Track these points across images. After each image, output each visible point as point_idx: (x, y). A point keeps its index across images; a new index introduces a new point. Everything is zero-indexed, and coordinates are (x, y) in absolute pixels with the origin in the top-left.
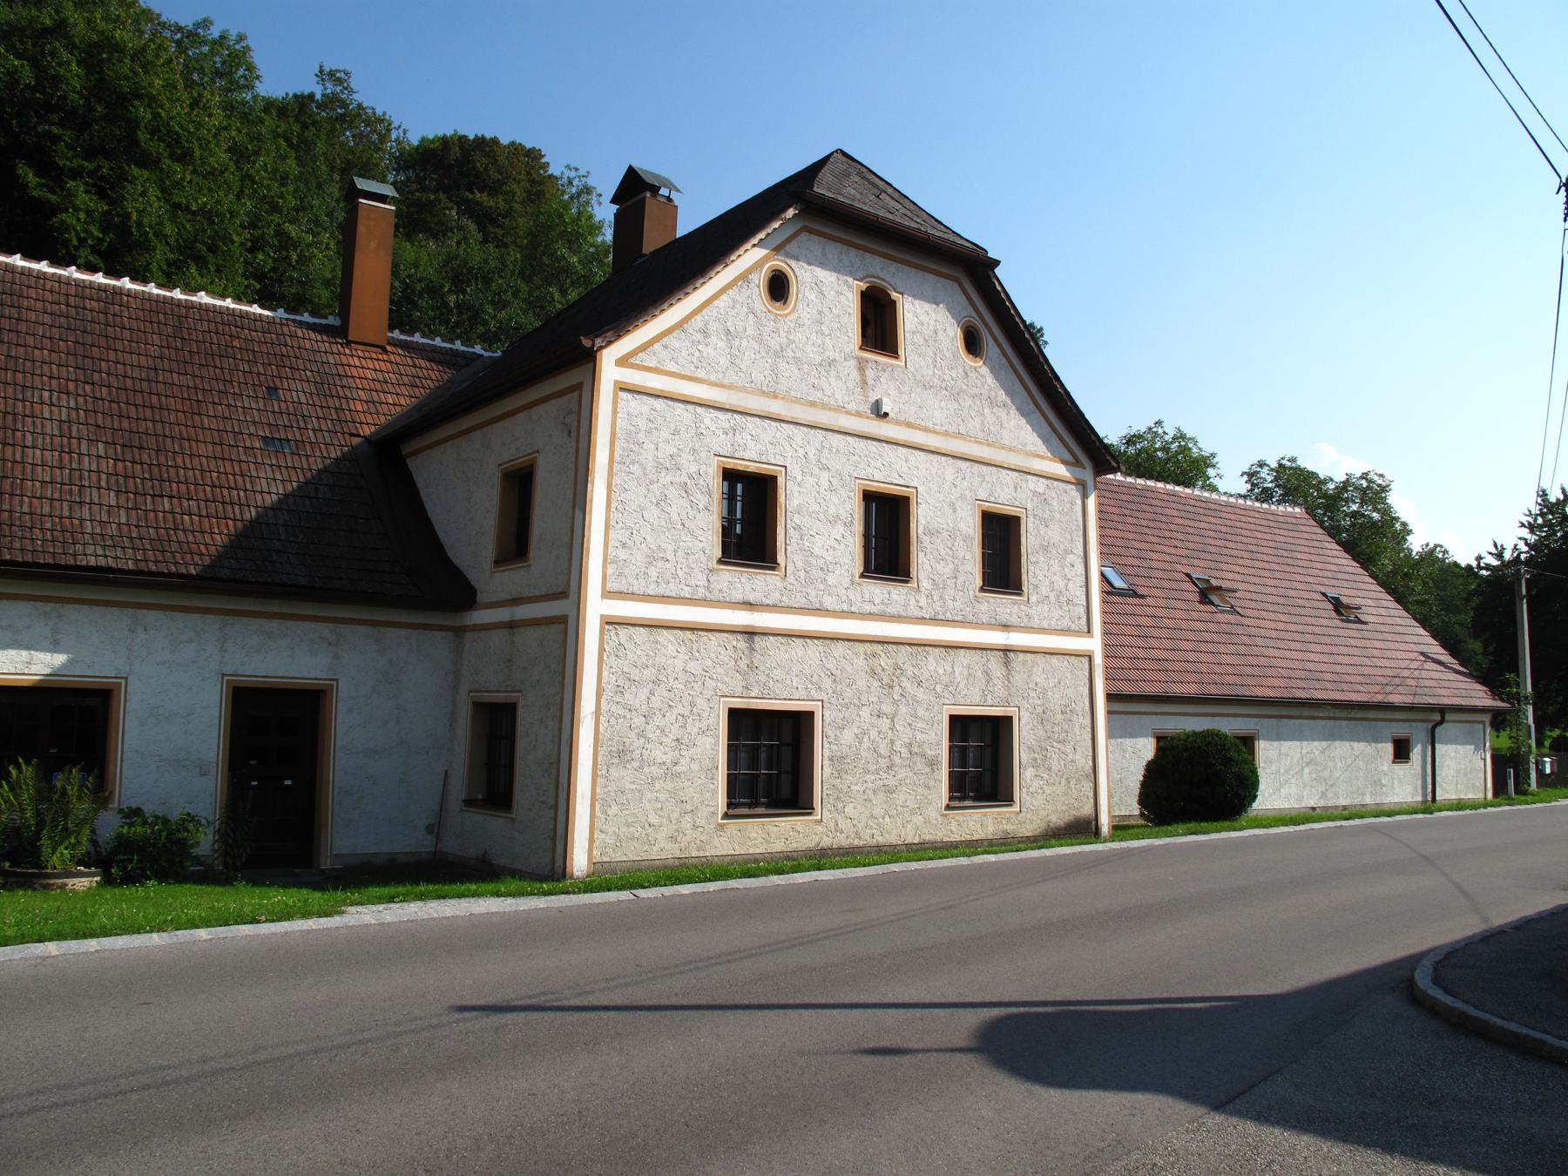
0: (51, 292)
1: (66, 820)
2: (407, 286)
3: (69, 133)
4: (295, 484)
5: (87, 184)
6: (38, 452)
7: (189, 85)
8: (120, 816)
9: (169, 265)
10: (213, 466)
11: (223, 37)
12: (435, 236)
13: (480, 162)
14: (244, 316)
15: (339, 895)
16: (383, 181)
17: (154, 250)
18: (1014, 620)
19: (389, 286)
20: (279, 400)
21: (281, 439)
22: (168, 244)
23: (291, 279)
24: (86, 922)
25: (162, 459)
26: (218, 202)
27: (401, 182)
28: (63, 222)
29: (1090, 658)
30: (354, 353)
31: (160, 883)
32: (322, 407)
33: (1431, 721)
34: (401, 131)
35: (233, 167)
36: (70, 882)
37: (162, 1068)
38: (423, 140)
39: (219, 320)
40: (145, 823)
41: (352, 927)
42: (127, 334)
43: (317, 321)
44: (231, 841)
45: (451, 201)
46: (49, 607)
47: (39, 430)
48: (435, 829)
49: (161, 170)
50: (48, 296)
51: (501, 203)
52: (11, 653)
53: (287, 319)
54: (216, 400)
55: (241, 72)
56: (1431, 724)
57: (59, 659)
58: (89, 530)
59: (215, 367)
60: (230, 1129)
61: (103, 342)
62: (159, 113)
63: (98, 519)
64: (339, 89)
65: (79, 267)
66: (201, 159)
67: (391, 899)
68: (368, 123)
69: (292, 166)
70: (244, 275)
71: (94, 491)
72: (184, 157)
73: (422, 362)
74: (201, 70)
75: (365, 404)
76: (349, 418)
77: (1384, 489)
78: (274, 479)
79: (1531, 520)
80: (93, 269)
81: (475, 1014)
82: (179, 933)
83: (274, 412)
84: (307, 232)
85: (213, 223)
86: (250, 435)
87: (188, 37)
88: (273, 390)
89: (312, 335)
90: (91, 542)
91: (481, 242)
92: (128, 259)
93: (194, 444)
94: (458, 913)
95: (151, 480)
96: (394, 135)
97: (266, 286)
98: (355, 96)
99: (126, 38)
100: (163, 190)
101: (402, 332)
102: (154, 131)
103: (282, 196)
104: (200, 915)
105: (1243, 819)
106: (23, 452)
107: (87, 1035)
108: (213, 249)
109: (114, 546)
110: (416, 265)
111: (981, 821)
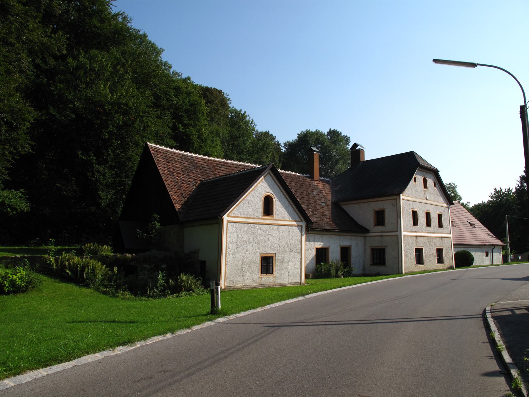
18: (442, 232)
29: (451, 238)
33: (491, 248)
46: (321, 235)
56: (492, 249)
77: (455, 187)
79: (492, 195)
105: (471, 266)
111: (440, 266)
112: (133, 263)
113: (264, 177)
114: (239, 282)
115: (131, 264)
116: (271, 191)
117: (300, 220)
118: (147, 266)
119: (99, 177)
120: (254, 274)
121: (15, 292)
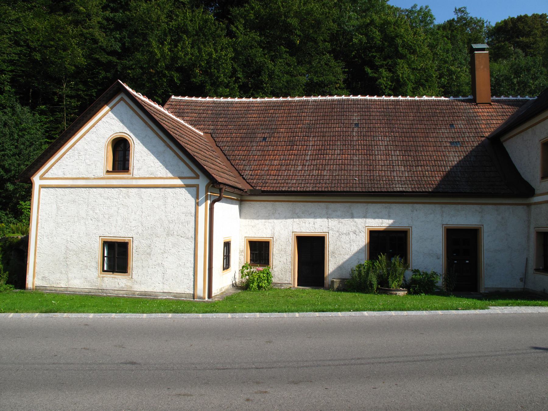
0: (378, 105)
1: (396, 273)
2: (497, 79)
3: (378, 54)
4: (462, 157)
5: (385, 68)
6: (379, 156)
7: (412, 28)
8: (412, 272)
9: (413, 89)
10: (434, 154)
11: (421, 9)
12: (506, 58)
13: (520, 25)
14: (439, 101)
15: (487, 302)
16: (483, 43)
17: (408, 85)
19: (489, 81)
20: (454, 128)
21: (456, 142)
22: (412, 82)
23: (454, 85)
24: (403, 306)
25: (417, 154)
26: (427, 65)
27: (490, 41)
28: (380, 82)
30: (479, 107)
31: (426, 295)
32: (470, 128)
34: (488, 23)
35: (430, 51)
36: (398, 293)
37: (427, 355)
38: (497, 24)
39: (431, 104)
40: (420, 275)
41: (492, 314)
42: (402, 114)
43: (465, 98)
44: (448, 282)
45: (511, 44)
46: (386, 205)
47: (379, 149)
48: (524, 279)
49: (407, 58)
50: (378, 107)
51: (531, 39)
52: (377, 220)
53: (454, 100)
54: (433, 132)
55: (428, 19)
57: (391, 221)
58: (396, 180)
59: (431, 120)
60: (450, 379)
61: (395, 118)
62: (404, 40)
63: (399, 175)
64: (463, 14)
65: (386, 96)
66: (419, 51)
67: (507, 305)
68: (475, 23)
69: (450, 46)
70: (438, 87)
71: (397, 166)
72: (414, 52)
73: (505, 106)
74: (416, 22)
75: (485, 125)
76: (480, 131)
78: (455, 156)
80: (389, 95)
81: (541, 351)
82: (432, 311)
83: (453, 133)
84: (458, 68)
85: (426, 72)
86: (445, 142)
87: (410, 12)
88: (452, 125)
89: (463, 103)
90: (397, 183)
91: (524, 56)
92: (400, 90)
93: (427, 147)
94: (533, 312)
95: (414, 161)
96: (485, 25)
97: (446, 89)
98: (469, 15)
99: (391, 19)
100: (409, 65)
101: (497, 96)
102: (403, 46)
103: (448, 57)
104: (439, 306)
106: (375, 157)
107: (404, 341)
108: (427, 81)
109: (405, 184)
110: (499, 71)
113: (112, 108)
114: (58, 281)
116: (126, 130)
117: (193, 175)
120: (87, 270)
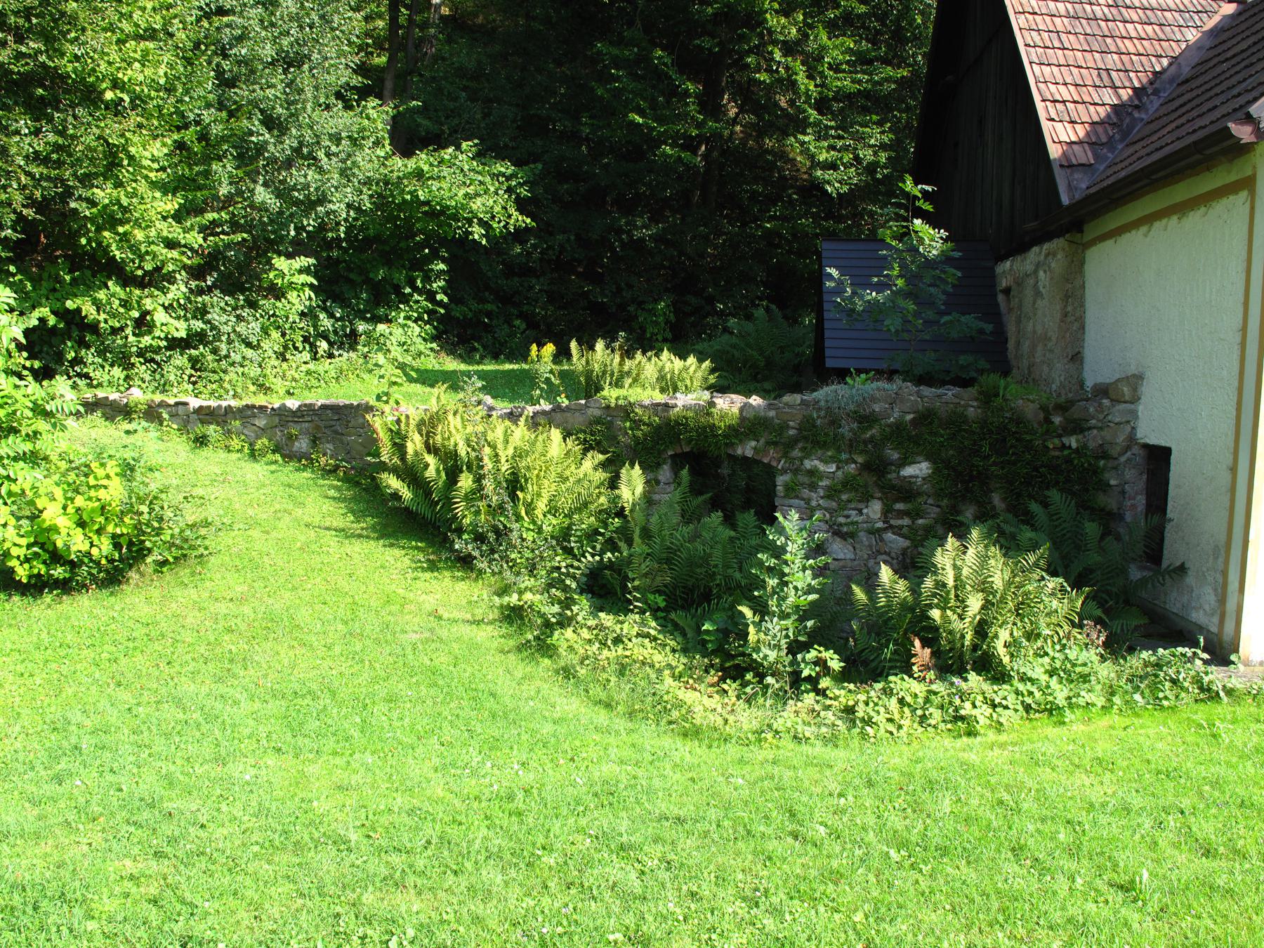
112: (747, 449)
115: (739, 452)
118: (822, 467)
119: (787, 68)
121: (65, 587)
